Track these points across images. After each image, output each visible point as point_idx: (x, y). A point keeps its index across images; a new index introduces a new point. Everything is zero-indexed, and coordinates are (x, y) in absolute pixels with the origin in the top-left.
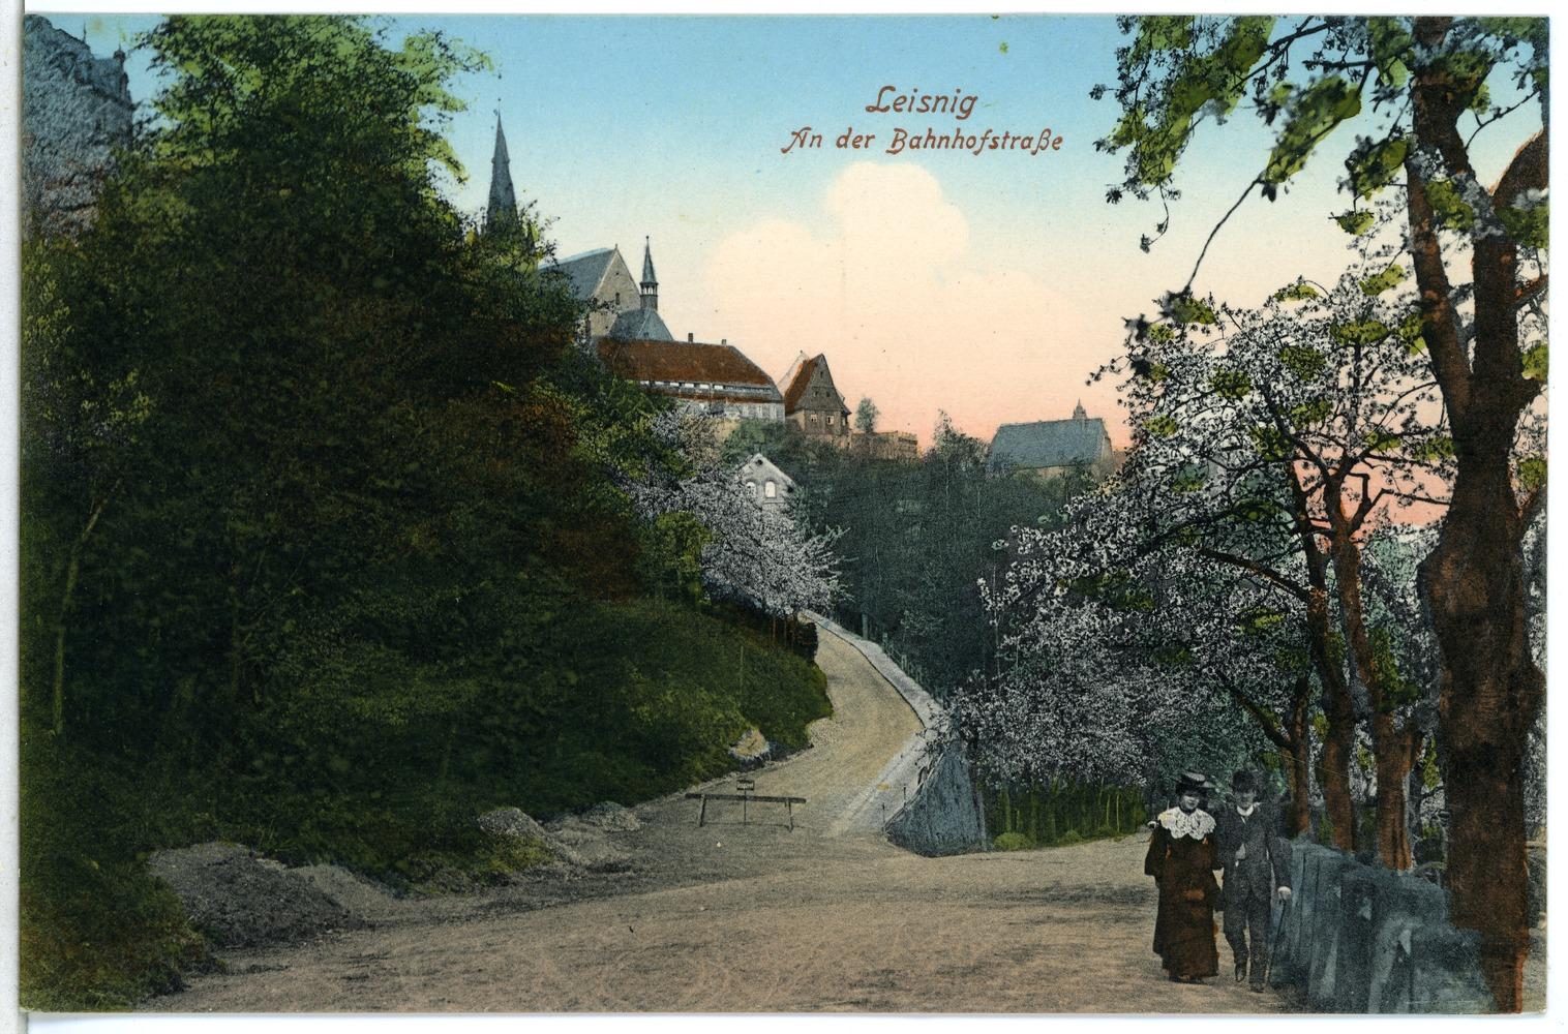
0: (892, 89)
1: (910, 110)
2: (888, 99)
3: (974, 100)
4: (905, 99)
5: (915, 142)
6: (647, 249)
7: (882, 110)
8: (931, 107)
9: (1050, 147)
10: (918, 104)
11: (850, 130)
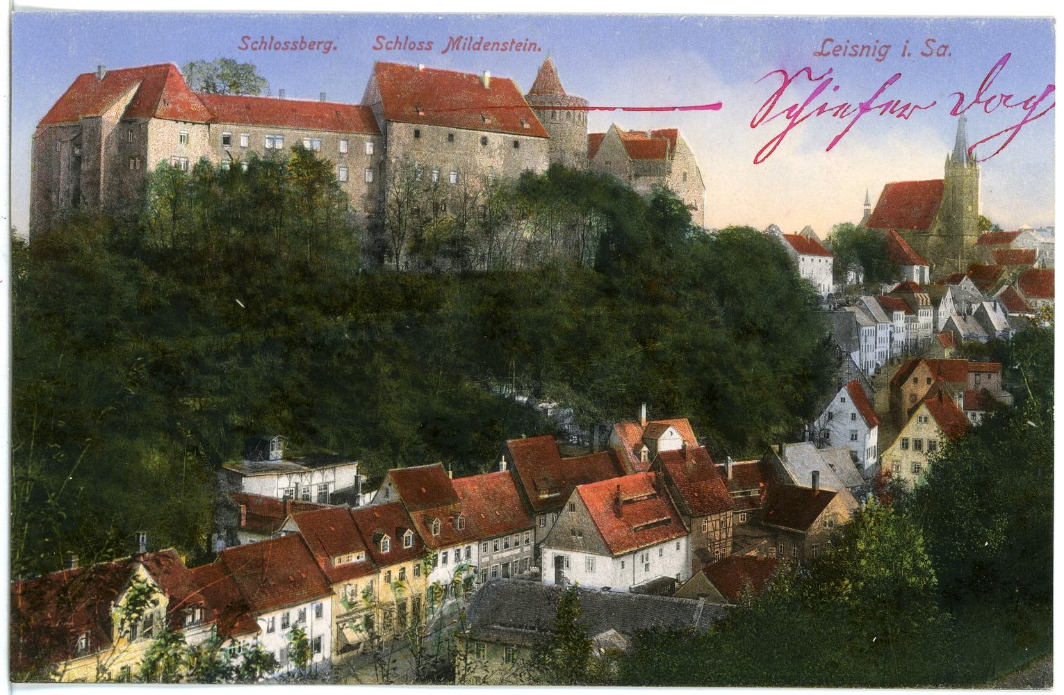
0: (831, 40)
1: (844, 55)
2: (829, 47)
3: (889, 47)
4: (841, 47)
5: (476, 46)
6: (624, 109)
7: (824, 55)
8: (859, 52)
9: (307, 48)
10: (850, 50)
11: (482, 38)
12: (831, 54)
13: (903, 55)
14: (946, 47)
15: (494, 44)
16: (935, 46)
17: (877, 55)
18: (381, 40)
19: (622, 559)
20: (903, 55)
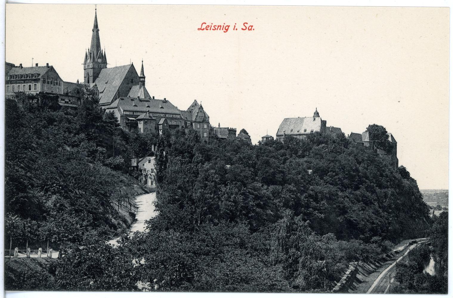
0: (205, 23)
2: (204, 26)
4: (209, 26)
10: (213, 28)
12: (205, 29)
13: (234, 29)
14: (252, 26)
15: (218, 26)
16: (247, 26)
17: (224, 30)
18: (215, 27)
19: (298, 133)
20: (234, 29)
